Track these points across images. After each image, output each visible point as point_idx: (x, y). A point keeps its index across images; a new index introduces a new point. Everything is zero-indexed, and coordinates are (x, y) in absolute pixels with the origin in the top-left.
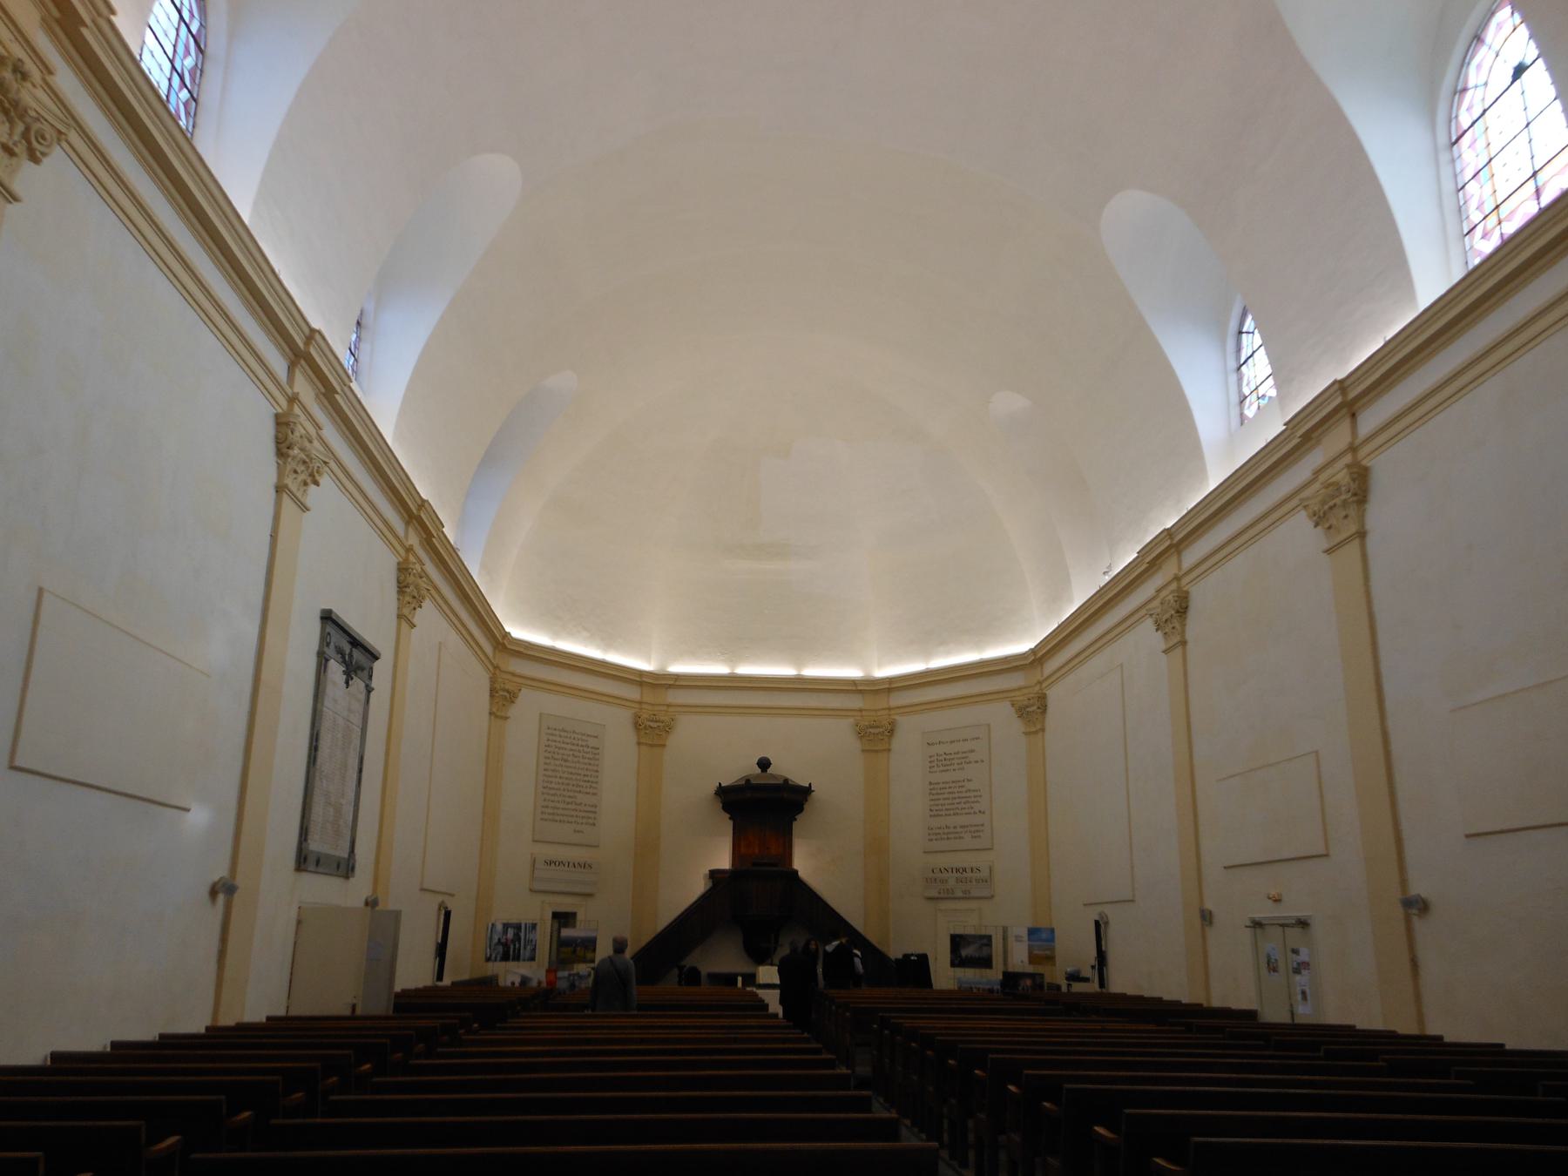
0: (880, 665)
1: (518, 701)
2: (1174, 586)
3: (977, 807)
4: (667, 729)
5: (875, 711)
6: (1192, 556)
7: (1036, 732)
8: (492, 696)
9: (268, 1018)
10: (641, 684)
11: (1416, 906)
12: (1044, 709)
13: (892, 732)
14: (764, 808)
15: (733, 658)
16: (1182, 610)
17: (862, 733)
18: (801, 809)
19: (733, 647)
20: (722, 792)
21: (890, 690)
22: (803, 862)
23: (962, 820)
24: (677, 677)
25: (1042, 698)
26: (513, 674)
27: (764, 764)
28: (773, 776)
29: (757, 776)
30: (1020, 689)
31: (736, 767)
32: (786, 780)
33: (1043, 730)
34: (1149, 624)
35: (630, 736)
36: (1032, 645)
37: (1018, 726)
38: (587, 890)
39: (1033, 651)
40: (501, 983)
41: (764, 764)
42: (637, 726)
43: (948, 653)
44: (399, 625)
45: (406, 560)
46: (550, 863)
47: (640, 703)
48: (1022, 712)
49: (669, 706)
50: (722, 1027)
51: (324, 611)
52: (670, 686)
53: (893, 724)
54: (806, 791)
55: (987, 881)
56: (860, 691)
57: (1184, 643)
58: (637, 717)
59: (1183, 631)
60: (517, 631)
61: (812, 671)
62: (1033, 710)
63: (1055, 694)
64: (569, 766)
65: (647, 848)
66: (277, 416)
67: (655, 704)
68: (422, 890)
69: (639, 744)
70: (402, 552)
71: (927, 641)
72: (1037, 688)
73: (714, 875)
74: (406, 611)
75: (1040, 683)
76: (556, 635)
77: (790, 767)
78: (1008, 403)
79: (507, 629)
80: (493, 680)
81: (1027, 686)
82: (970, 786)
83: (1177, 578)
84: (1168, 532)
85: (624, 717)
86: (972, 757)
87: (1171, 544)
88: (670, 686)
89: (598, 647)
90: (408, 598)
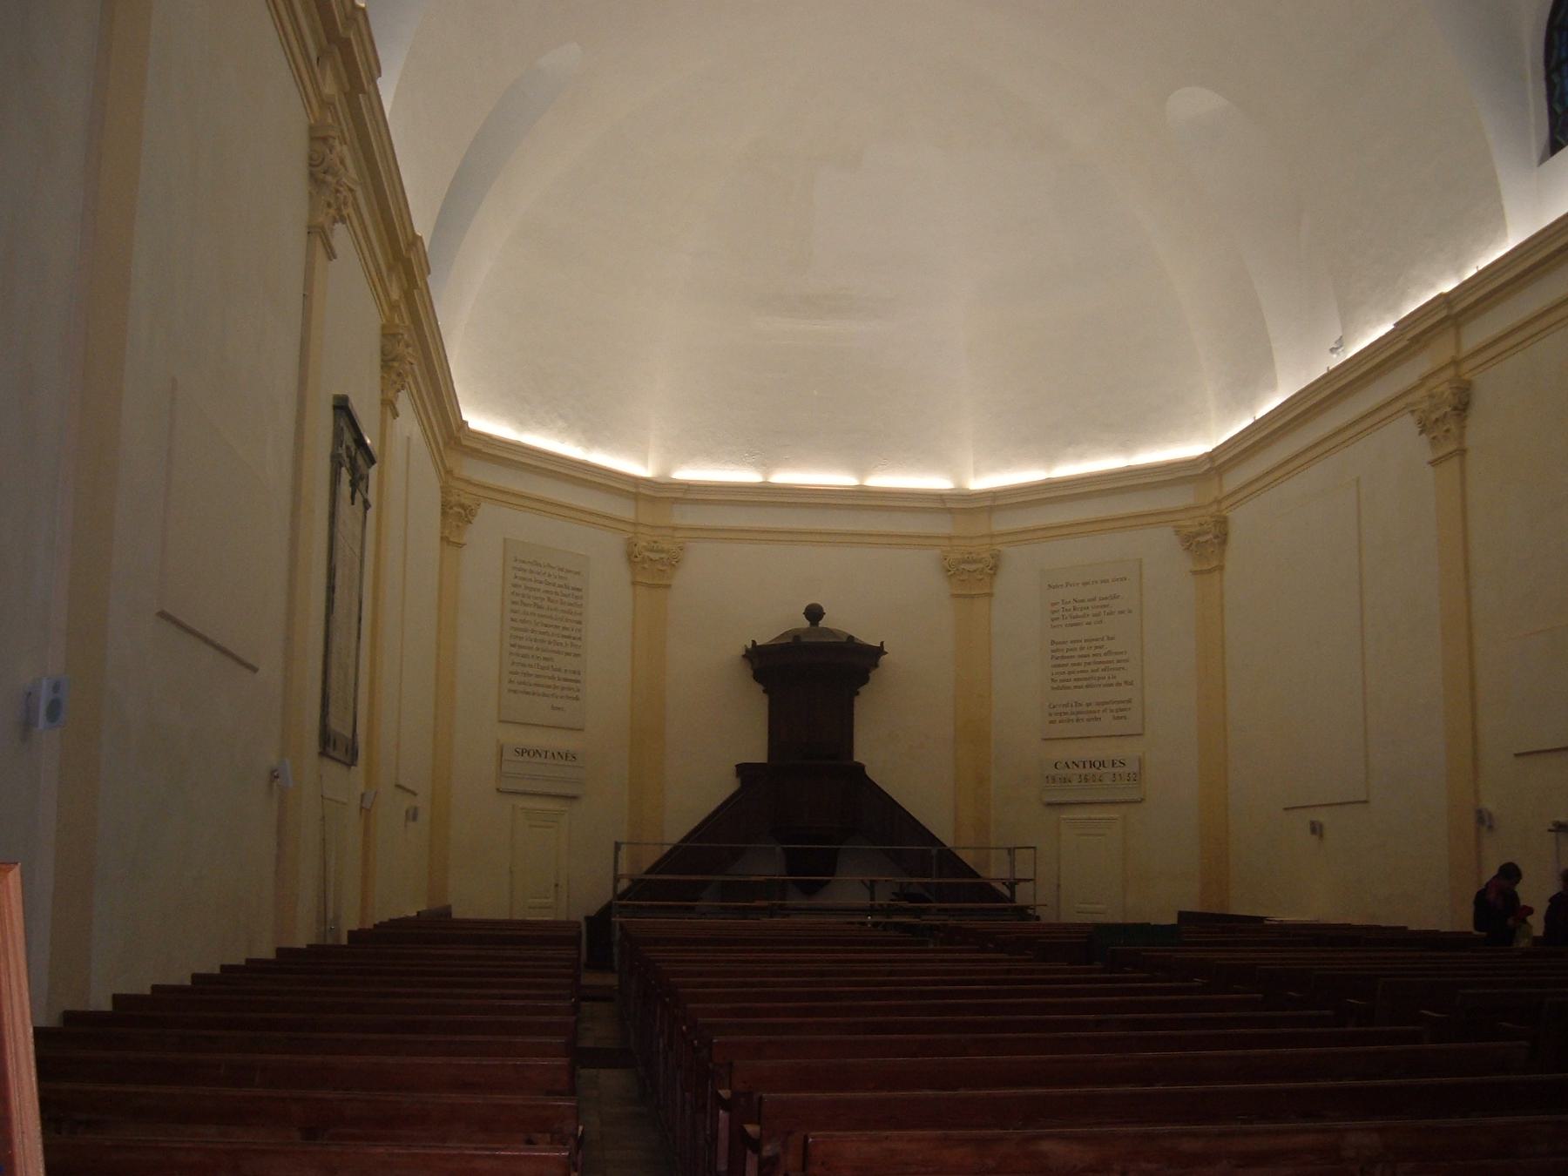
0: (977, 472)
1: (476, 520)
2: (1450, 373)
4: (673, 562)
5: (969, 539)
6: (1477, 334)
7: (1210, 571)
8: (444, 513)
9: (247, 960)
10: (636, 497)
11: (1483, 819)
12: (1223, 538)
13: (995, 568)
14: (813, 676)
15: (767, 460)
16: (1462, 407)
17: (952, 571)
18: (864, 680)
19: (768, 442)
21: (991, 510)
24: (688, 487)
25: (1222, 523)
26: (468, 482)
27: (814, 613)
28: (830, 632)
29: (807, 632)
30: (1187, 509)
31: (775, 619)
32: (851, 638)
33: (1221, 568)
34: (1408, 424)
36: (1208, 448)
38: (568, 790)
39: (1210, 456)
40: (455, 916)
41: (814, 613)
42: (632, 558)
43: (1081, 457)
44: (383, 413)
46: (524, 752)
47: (635, 524)
48: (1190, 542)
49: (675, 528)
50: (907, 961)
51: (336, 398)
52: (676, 500)
53: (997, 557)
54: (879, 651)
55: (1136, 777)
56: (950, 510)
57: (1462, 452)
58: (631, 545)
59: (1462, 436)
60: (478, 421)
61: (881, 480)
62: (1207, 542)
63: (1241, 519)
66: (311, 128)
67: (656, 523)
68: (398, 786)
69: (634, 583)
71: (1049, 442)
72: (1214, 508)
73: (743, 770)
74: (390, 394)
75: (1218, 502)
76: (522, 424)
78: (1195, 103)
79: (465, 417)
80: (445, 491)
81: (1197, 511)
83: (1455, 363)
84: (1444, 299)
87: (1448, 315)
88: (676, 500)
89: (579, 443)
90: (394, 377)
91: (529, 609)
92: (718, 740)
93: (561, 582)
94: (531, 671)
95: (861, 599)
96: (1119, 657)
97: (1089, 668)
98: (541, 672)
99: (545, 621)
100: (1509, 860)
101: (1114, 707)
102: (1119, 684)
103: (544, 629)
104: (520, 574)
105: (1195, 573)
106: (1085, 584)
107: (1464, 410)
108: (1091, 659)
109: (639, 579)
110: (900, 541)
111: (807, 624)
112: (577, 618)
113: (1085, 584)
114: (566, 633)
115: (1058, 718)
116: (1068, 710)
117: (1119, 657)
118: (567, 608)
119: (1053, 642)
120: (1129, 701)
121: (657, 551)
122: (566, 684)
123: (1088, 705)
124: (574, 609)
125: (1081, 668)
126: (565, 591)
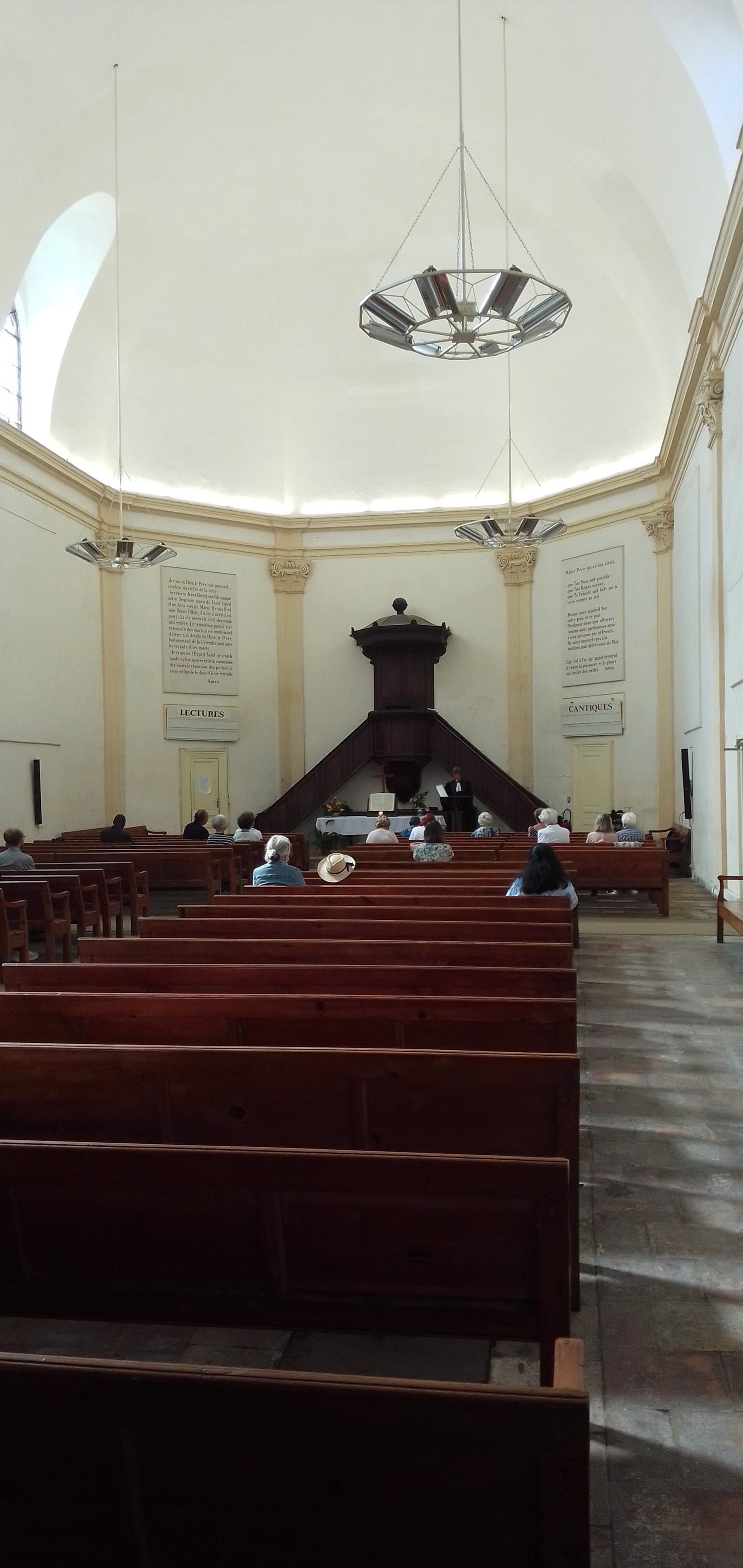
3: (611, 637)
4: (306, 575)
10: (274, 529)
13: (533, 562)
18: (442, 651)
20: (358, 635)
22: (445, 705)
23: (598, 651)
27: (400, 605)
30: (652, 504)
31: (376, 610)
32: (414, 621)
35: (267, 585)
37: (650, 544)
41: (400, 605)
45: (100, 530)
47: (274, 550)
48: (653, 530)
49: (304, 550)
52: (304, 530)
64: (199, 629)
65: (289, 697)
67: (288, 552)
69: (276, 591)
70: (96, 525)
77: (428, 609)
82: (603, 614)
85: (258, 565)
86: (607, 583)
88: (304, 530)
91: (184, 615)
92: (343, 698)
93: (213, 594)
94: (188, 657)
95: (448, 591)
96: (610, 623)
97: (591, 632)
98: (197, 658)
99: (200, 622)
100: (21, 829)
101: (606, 660)
102: (609, 643)
103: (199, 628)
104: (174, 590)
105: (656, 553)
106: (588, 568)
107: (721, 399)
108: (591, 626)
109: (280, 588)
110: (361, 551)
111: (395, 613)
112: (227, 619)
113: (588, 568)
114: (218, 629)
115: (572, 671)
116: (577, 664)
117: (610, 623)
118: (217, 612)
119: (569, 615)
120: (616, 656)
121: (291, 568)
122: (221, 665)
123: (590, 660)
124: (223, 613)
125: (586, 633)
126: (215, 600)
